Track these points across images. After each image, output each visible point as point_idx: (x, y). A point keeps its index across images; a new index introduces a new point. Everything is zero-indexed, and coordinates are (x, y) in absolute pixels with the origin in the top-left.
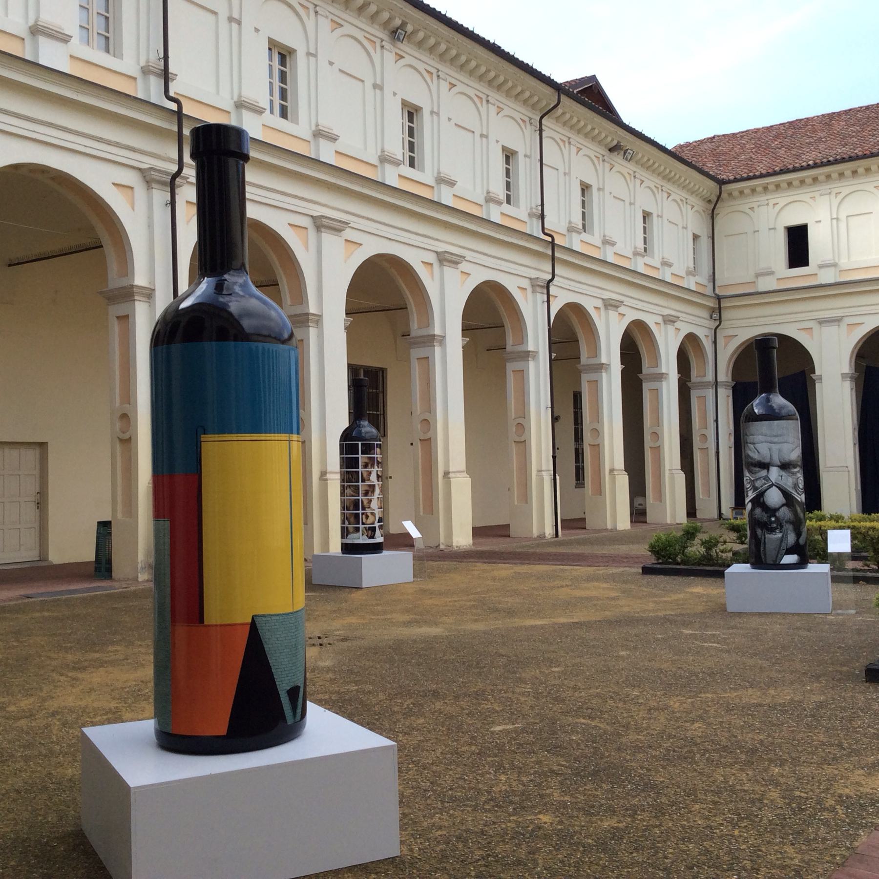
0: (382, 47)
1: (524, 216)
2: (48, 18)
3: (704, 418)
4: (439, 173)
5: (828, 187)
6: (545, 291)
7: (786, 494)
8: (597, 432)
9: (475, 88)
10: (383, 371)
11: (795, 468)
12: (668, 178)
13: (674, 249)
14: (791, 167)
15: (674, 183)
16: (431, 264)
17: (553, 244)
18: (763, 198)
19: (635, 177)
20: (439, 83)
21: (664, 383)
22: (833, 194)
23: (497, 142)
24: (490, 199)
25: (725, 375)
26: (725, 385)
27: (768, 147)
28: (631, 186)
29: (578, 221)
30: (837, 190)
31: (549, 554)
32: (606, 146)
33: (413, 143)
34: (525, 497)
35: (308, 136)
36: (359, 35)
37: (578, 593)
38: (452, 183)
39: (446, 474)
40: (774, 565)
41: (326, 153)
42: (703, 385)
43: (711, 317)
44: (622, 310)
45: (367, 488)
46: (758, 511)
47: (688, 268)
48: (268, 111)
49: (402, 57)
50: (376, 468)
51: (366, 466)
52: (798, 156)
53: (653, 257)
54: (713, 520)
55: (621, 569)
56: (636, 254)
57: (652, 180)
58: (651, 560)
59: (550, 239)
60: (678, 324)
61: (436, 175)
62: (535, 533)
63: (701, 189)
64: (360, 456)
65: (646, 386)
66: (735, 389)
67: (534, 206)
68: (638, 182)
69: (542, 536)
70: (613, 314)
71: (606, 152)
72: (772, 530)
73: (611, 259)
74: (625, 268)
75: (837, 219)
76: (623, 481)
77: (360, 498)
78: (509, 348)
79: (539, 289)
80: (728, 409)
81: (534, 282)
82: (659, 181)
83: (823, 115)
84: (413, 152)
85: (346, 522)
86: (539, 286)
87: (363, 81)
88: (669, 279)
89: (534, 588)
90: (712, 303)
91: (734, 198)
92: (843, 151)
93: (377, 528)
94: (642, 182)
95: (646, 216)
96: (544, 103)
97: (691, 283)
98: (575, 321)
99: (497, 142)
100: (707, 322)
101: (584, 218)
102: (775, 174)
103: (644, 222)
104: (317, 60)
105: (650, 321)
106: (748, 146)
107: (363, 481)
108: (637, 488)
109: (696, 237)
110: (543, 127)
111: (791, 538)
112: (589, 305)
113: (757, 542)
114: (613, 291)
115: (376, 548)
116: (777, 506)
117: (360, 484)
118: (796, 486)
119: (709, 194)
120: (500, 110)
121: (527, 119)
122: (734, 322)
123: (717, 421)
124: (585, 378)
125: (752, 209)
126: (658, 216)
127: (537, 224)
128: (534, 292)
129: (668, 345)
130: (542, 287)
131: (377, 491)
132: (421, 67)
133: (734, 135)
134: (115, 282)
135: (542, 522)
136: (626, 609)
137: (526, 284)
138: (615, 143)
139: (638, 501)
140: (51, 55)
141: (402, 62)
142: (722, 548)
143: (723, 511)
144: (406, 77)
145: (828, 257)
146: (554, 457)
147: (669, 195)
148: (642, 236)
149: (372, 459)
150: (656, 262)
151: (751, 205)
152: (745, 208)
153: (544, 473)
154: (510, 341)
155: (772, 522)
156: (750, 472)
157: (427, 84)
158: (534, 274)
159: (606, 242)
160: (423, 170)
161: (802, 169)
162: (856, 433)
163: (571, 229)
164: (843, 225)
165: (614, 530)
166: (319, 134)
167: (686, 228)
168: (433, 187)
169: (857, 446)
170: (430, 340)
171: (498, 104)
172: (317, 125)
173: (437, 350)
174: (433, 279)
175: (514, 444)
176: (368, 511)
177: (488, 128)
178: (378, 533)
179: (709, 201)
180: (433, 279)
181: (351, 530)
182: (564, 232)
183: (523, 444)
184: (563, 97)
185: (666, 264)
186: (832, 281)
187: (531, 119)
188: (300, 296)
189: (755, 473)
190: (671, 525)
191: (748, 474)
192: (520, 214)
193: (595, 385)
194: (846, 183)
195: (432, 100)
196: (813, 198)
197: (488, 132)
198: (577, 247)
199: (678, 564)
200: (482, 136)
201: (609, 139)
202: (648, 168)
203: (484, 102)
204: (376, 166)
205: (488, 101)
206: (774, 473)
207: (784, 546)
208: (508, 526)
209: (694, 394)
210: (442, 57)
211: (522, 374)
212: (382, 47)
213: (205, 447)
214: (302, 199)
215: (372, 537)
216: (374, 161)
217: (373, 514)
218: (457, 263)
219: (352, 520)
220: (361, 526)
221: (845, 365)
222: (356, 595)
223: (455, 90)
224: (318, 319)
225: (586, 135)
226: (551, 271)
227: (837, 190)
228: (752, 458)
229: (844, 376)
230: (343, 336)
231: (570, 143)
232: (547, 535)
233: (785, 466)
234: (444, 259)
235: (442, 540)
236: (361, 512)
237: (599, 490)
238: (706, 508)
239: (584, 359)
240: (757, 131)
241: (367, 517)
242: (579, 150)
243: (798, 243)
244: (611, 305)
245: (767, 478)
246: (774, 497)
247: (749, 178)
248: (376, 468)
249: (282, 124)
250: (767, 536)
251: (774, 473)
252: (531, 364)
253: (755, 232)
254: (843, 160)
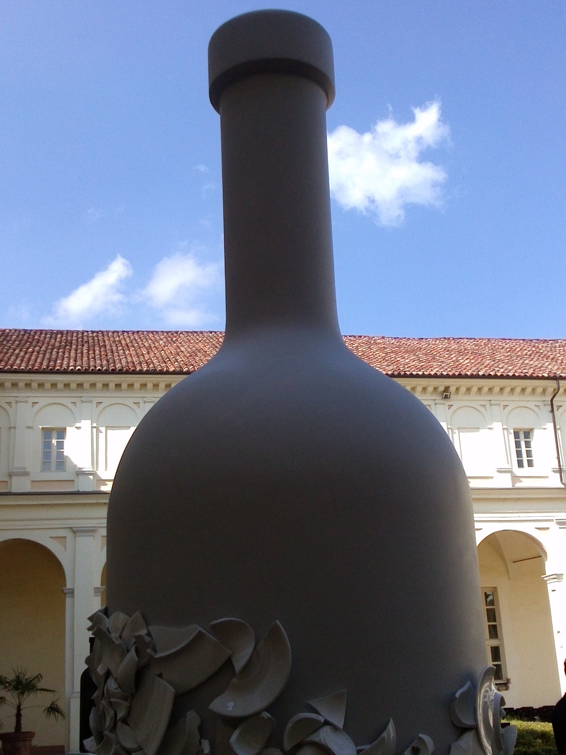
18: (23, 394)
36: (521, 404)
125: (9, 403)
151: (9, 400)
194: (109, 395)
213: (110, 490)
227: (99, 400)
253: (10, 428)
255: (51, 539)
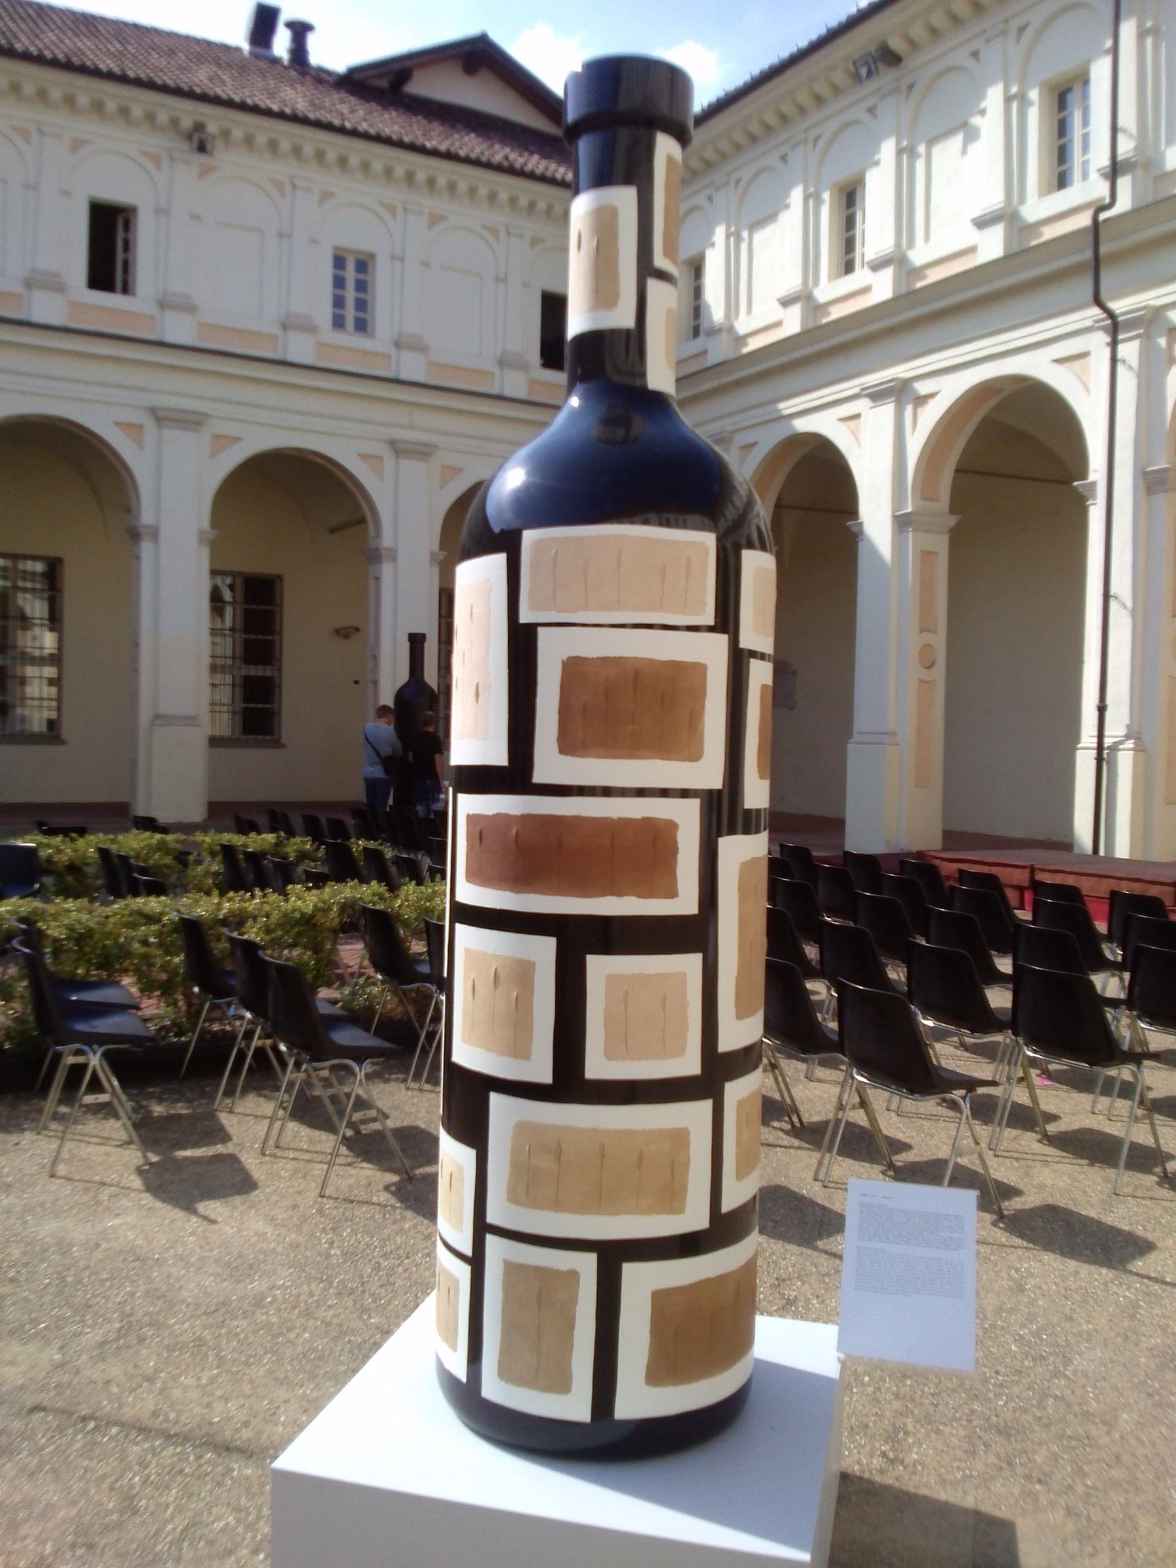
140: (300, 349)
205: (294, 186)
224: (154, 534)
249: (349, 339)
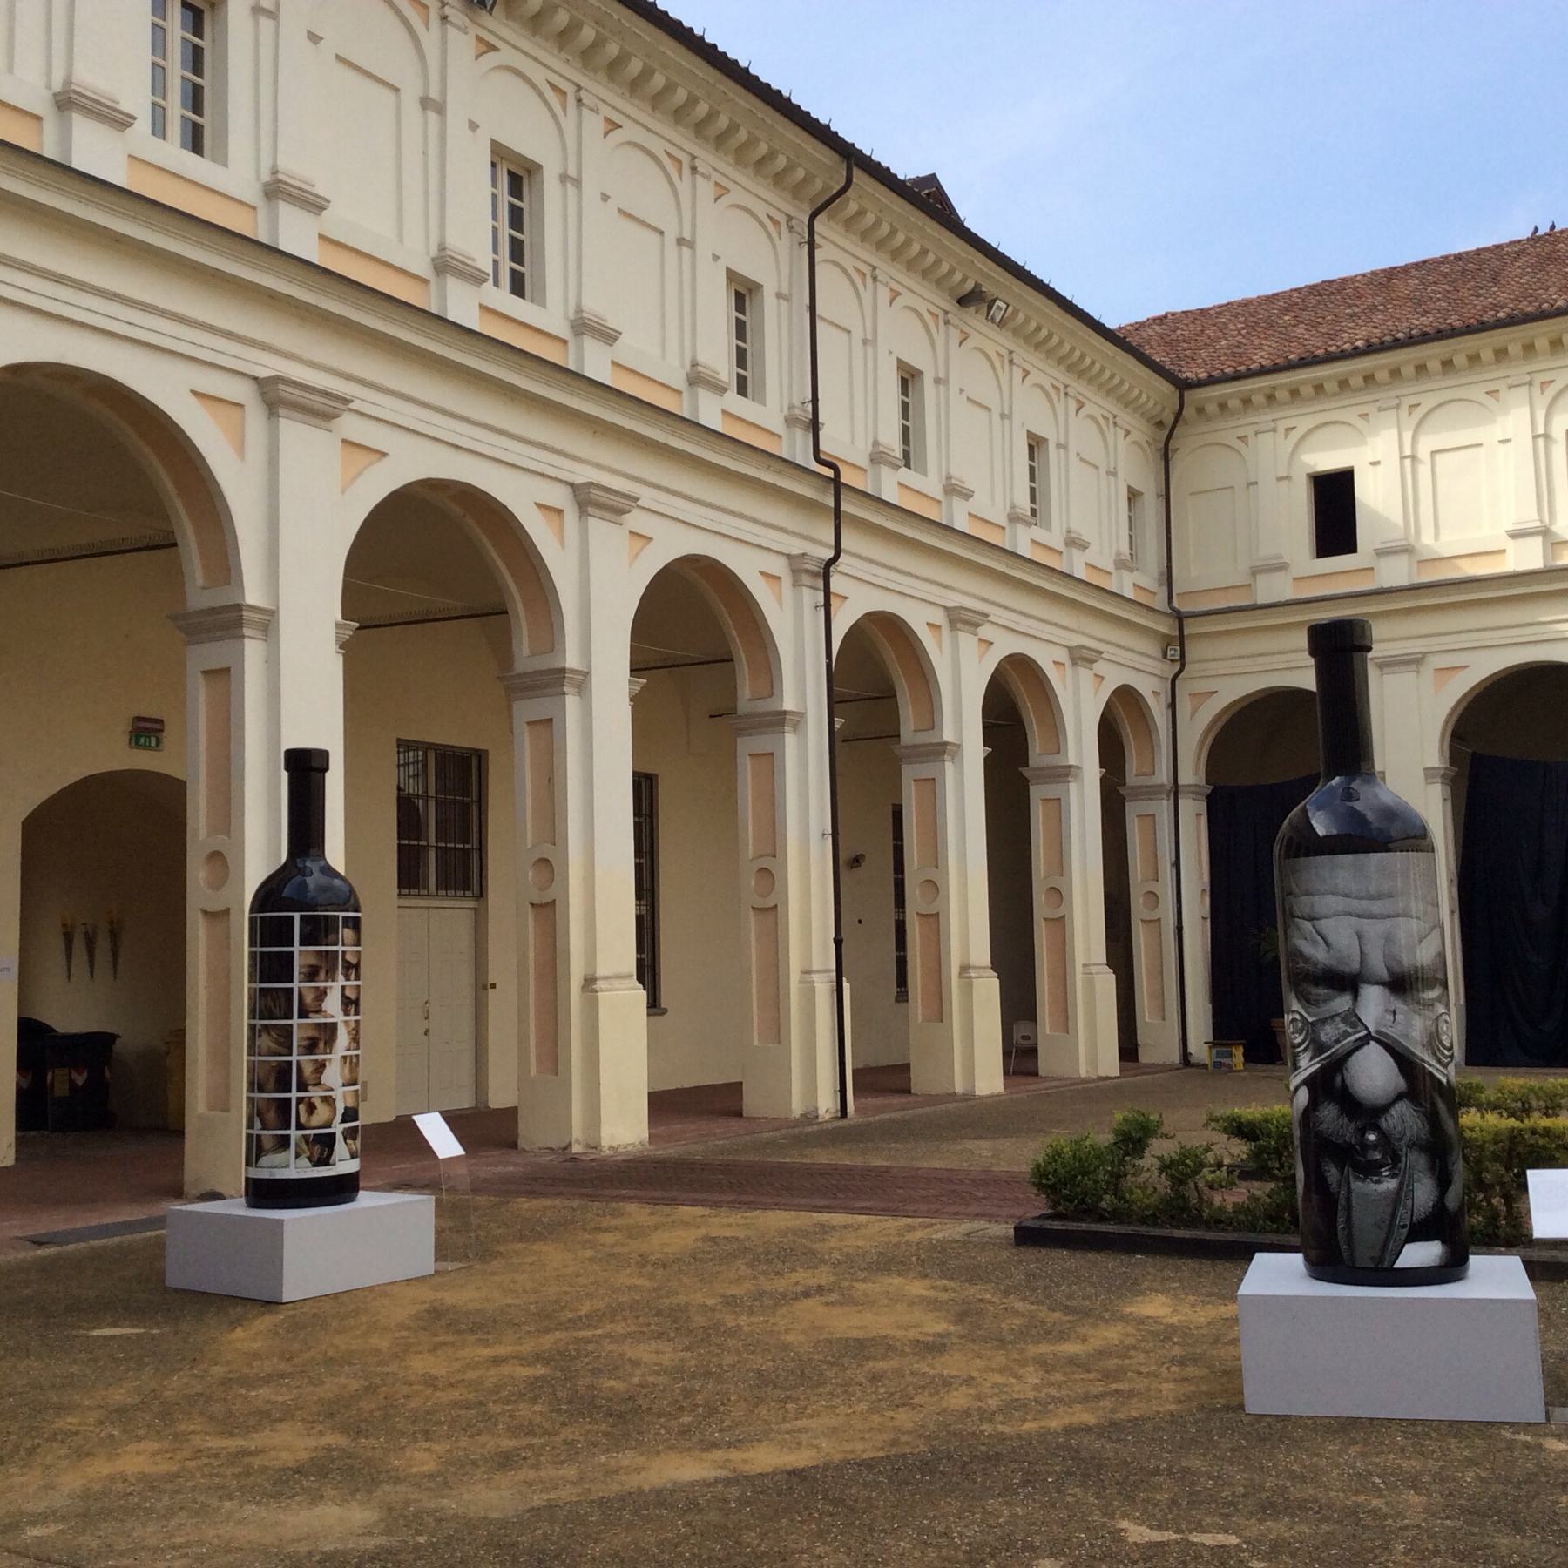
0: (444, 18)
1: (776, 423)
2: (92, 78)
3: (1153, 857)
4: (579, 310)
5: (1393, 393)
6: (821, 584)
7: (1404, 1061)
8: (934, 887)
9: (668, 137)
10: (480, 756)
11: (1432, 987)
12: (1077, 369)
13: (1091, 515)
14: (1320, 352)
15: (1090, 381)
16: (560, 512)
17: (837, 484)
18: (1265, 417)
19: (1011, 361)
20: (580, 115)
21: (1073, 787)
22: (1405, 407)
23: (716, 258)
24: (698, 379)
25: (1192, 773)
26: (1194, 791)
27: (1272, 325)
28: (1004, 379)
29: (892, 440)
30: (1413, 400)
31: (811, 1172)
32: (951, 291)
33: (521, 243)
34: (776, 1028)
35: (252, 194)
37: (846, 1323)
38: (610, 337)
39: (589, 982)
40: (1376, 1270)
41: (297, 234)
42: (1152, 792)
43: (1165, 656)
44: (986, 631)
45: (311, 1033)
46: (1329, 1114)
47: (1118, 554)
48: (143, 124)
49: (492, 48)
50: (341, 980)
51: (312, 974)
52: (1333, 336)
53: (1049, 529)
54: (1169, 1068)
55: (966, 1226)
56: (1014, 518)
57: (1046, 373)
58: (1035, 1208)
59: (829, 473)
60: (1100, 667)
61: (572, 316)
62: (797, 1108)
63: (1144, 397)
64: (297, 948)
65: (1037, 793)
66: (1211, 800)
67: (796, 402)
68: (1018, 373)
69: (810, 1117)
70: (967, 641)
71: (951, 306)
72: (1370, 1171)
73: (961, 524)
74: (993, 546)
75: (1413, 458)
76: (988, 990)
77: (294, 1058)
78: (743, 706)
79: (806, 579)
80: (1199, 843)
81: (796, 563)
82: (1061, 376)
83: (1374, 273)
84: (521, 263)
85: (258, 1124)
86: (807, 571)
87: (397, 90)
88: (1081, 573)
89: (731, 1302)
90: (1166, 627)
91: (1209, 419)
92: (1419, 322)
93: (339, 1138)
94: (1027, 373)
95: (1036, 445)
96: (819, 184)
97: (1125, 584)
98: (889, 655)
99: (716, 258)
100: (1159, 665)
101: (906, 439)
102: (1290, 366)
103: (1032, 458)
104: (277, 26)
105: (1045, 657)
106: (1231, 326)
107: (303, 1014)
108: (1019, 1004)
109: (1133, 495)
110: (818, 239)
111: (1424, 1194)
112: (917, 618)
113: (1327, 1201)
114: (967, 591)
115: (341, 1190)
116: (1384, 1102)
117: (295, 1021)
118: (1433, 1040)
119: (1159, 408)
120: (721, 192)
121: (782, 219)
122: (1204, 665)
123: (1177, 864)
124: (909, 773)
125: (1243, 438)
126: (1059, 446)
127: (803, 440)
128: (796, 584)
129: (1080, 707)
130: (815, 575)
131: (343, 1038)
132: (539, 76)
133: (1203, 312)
134: (200, 595)
135: (809, 1079)
136: (958, 1399)
137: (779, 567)
138: (969, 286)
139: (1021, 1030)
141: (491, 59)
142: (1210, 1177)
143: (1192, 1049)
144: (501, 95)
145: (1395, 537)
146: (838, 943)
147: (1081, 406)
148: (1026, 484)
149: (331, 957)
150: (1055, 539)
151: (1241, 432)
152: (1230, 438)
153: (815, 977)
154: (745, 691)
155: (1366, 1146)
156: (1306, 1000)
157: (554, 116)
158: (797, 546)
159: (953, 489)
160: (542, 303)
161: (1343, 356)
162: (1455, 890)
163: (878, 457)
164: (1424, 471)
165: (969, 1097)
166: (277, 190)
167: (1114, 474)
168: (565, 342)
169: (1457, 915)
170: (554, 681)
171: (715, 176)
172: (275, 172)
173: (572, 702)
174: (562, 544)
175: (751, 913)
176: (315, 1094)
177: (694, 225)
178: (341, 1148)
179: (1160, 424)
180: (562, 544)
181: (268, 1144)
182: (864, 462)
183: (772, 914)
184: (856, 171)
185: (1074, 542)
186: (1402, 581)
187: (790, 218)
188: (224, 564)
189: (1317, 1003)
190: (1085, 1081)
191: (1296, 1006)
192: (768, 415)
193: (931, 786)
195: (564, 148)
196: (1364, 416)
197: (694, 233)
198: (890, 494)
199: (1102, 1219)
200: (681, 241)
201: (958, 276)
202: (1037, 346)
203: (686, 171)
204: (425, 282)
205: (694, 169)
206: (1373, 1005)
207: (1404, 1218)
208: (736, 1088)
209: (1133, 811)
210: (587, 57)
211: (770, 762)
212: (444, 18)
214: (230, 335)
215: (324, 1161)
216: (422, 267)
217: (329, 1101)
218: (621, 512)
219: (271, 1116)
220: (294, 1133)
221: (1433, 753)
222: (248, 1338)
223: (617, 135)
224: (268, 623)
225: (910, 265)
226: (832, 542)
227: (1413, 400)
228: (1307, 960)
229: (1429, 773)
230: (334, 666)
231: (875, 279)
232: (822, 1112)
233: (1401, 984)
234: (590, 501)
235: (577, 1132)
236: (294, 1095)
237: (939, 1013)
238: (1159, 1045)
239: (909, 732)
240: (1246, 303)
241: (312, 1108)
242: (895, 295)
243: (1334, 500)
244: (967, 623)
245: (1352, 1019)
246: (1373, 1074)
247: (1237, 377)
248: (341, 980)
250: (1357, 1185)
251: (1373, 1005)
252: (790, 740)
254: (1425, 338)
255: (193, 399)
